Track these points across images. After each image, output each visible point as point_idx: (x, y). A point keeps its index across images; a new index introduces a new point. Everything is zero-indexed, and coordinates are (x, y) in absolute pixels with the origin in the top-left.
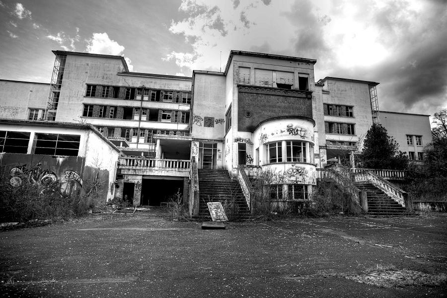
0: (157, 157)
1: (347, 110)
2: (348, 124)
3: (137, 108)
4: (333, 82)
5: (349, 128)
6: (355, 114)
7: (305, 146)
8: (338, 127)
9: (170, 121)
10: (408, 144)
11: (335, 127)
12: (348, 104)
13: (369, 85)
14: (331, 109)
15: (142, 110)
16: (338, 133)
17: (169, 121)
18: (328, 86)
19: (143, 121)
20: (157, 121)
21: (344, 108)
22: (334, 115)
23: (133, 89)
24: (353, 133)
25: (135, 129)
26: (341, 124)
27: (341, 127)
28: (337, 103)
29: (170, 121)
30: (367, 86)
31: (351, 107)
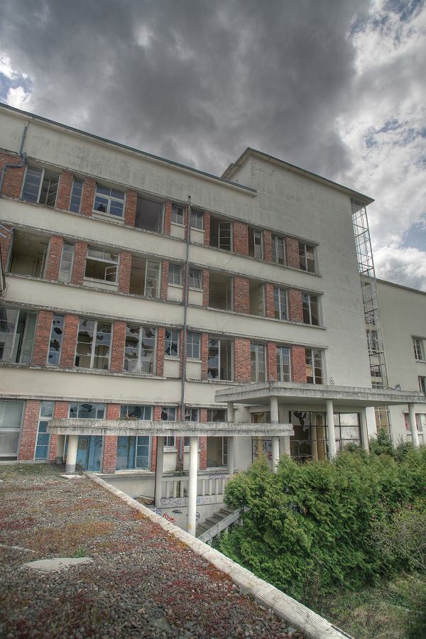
0: (214, 426)
1: (302, 253)
2: (305, 293)
3: (175, 266)
4: (268, 169)
5: (305, 305)
6: (321, 267)
7: (320, 375)
8: (276, 299)
9: (115, 289)
10: (416, 358)
11: (266, 296)
12: (305, 236)
13: (352, 201)
14: (258, 242)
15: (186, 272)
16: (277, 316)
17: (113, 286)
18: (253, 174)
19: (194, 306)
20: (36, 276)
21: (295, 246)
22: (266, 259)
23: (159, 202)
24: (315, 322)
25: (170, 332)
26: (285, 289)
27: (284, 301)
28: (276, 226)
29: (115, 289)
30: (347, 202)
31: (311, 247)
